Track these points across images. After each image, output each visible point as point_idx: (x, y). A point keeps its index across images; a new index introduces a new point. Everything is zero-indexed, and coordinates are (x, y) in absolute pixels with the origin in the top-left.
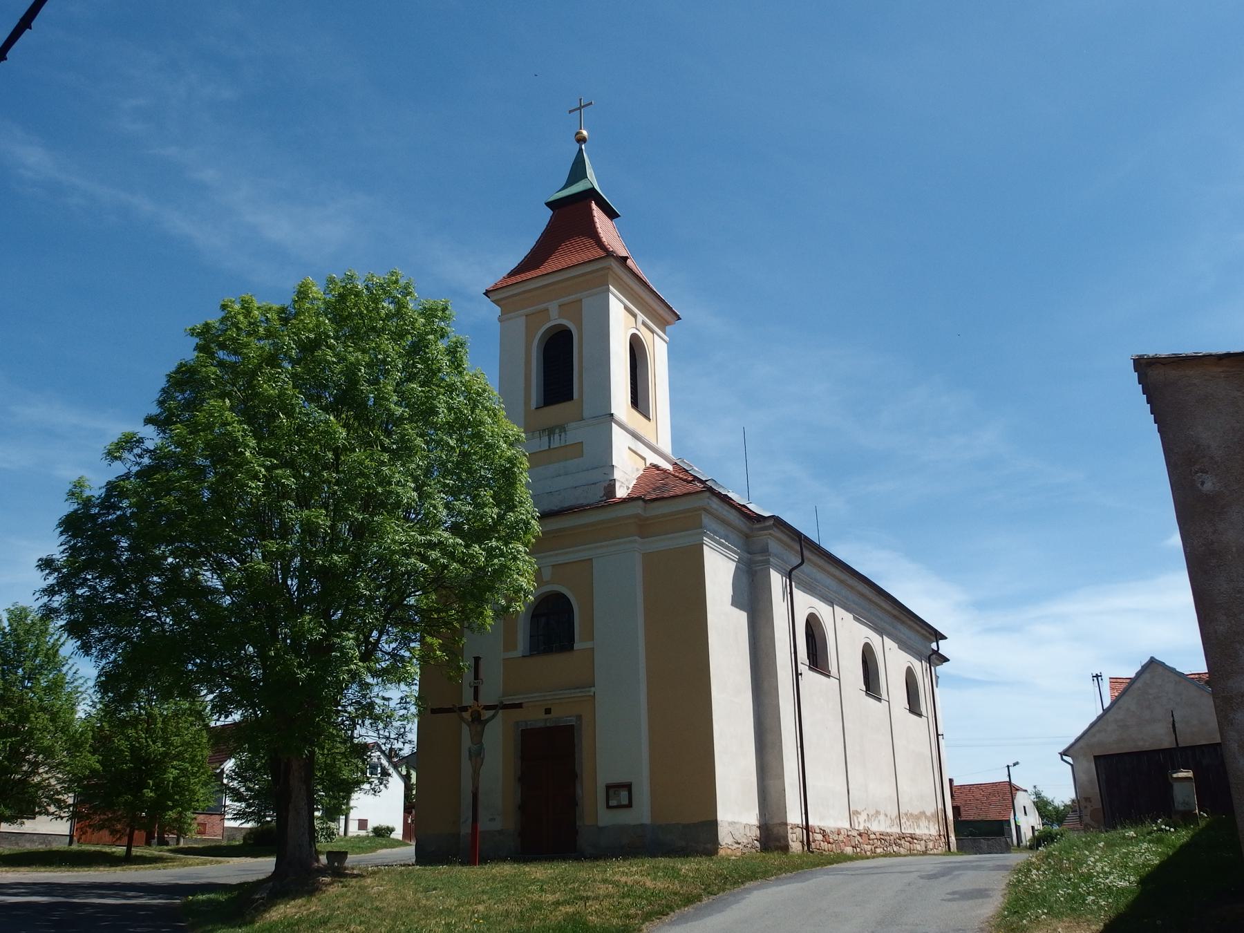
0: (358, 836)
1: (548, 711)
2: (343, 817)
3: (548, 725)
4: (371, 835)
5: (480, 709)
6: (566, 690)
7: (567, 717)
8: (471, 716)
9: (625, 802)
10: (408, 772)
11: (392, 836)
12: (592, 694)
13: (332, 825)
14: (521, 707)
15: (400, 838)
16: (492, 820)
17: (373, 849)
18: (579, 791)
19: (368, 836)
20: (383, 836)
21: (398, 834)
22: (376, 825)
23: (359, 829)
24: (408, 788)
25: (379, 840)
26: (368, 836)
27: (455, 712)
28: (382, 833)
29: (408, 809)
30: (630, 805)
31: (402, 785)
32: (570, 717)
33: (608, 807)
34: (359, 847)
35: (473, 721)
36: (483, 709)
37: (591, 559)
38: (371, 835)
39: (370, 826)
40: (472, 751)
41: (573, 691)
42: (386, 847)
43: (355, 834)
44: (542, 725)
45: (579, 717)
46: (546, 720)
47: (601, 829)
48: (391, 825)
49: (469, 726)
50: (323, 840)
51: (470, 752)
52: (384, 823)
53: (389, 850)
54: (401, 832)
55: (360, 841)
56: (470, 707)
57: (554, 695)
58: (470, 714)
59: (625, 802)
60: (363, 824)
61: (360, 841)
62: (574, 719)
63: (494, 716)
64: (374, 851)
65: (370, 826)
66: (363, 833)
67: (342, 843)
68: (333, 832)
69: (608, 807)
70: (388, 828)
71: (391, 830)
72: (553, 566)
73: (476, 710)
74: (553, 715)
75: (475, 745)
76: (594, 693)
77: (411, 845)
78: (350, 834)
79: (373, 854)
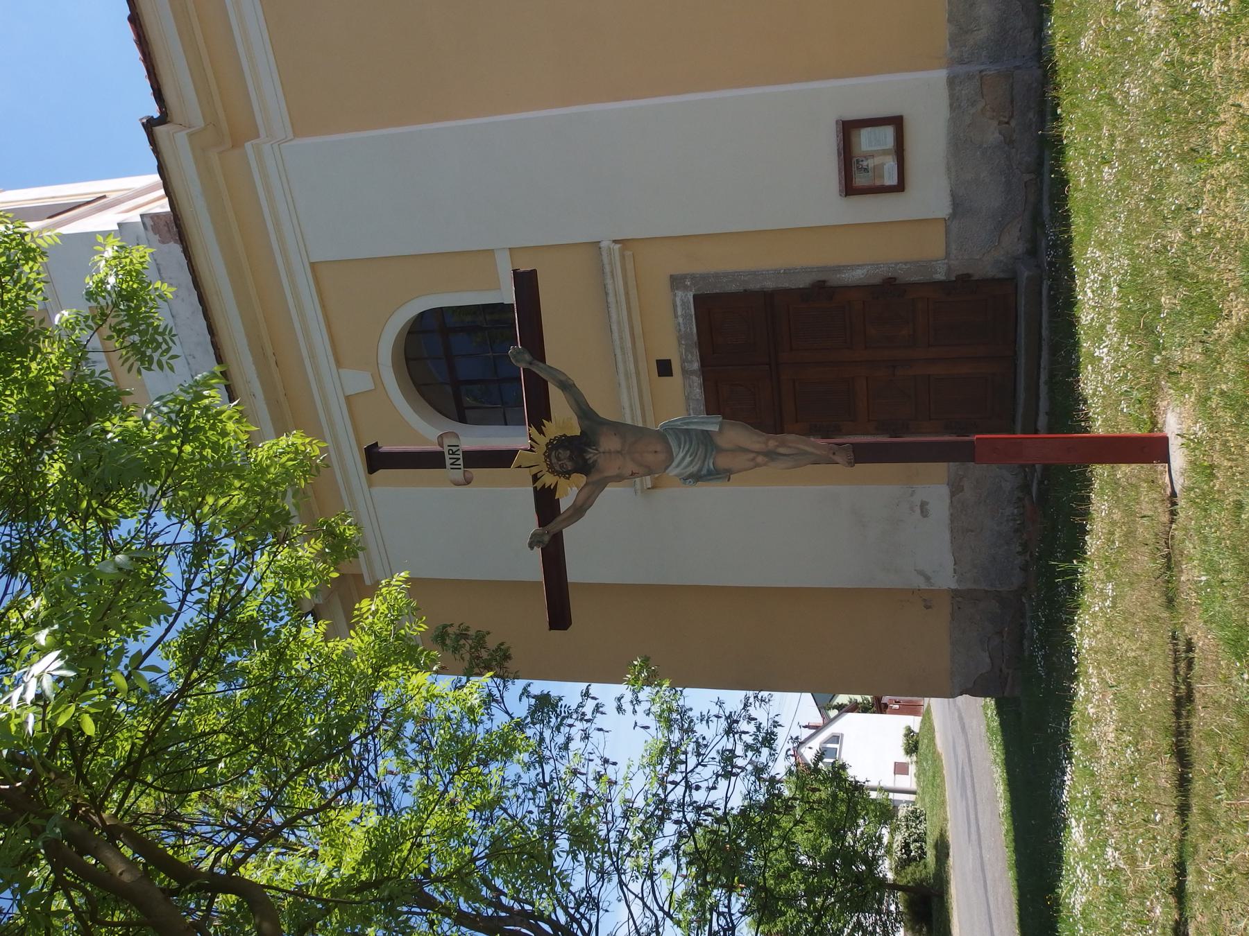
0: (918, 776)
1: (664, 368)
2: (891, 796)
3: (696, 366)
4: (914, 758)
5: (543, 441)
6: (610, 317)
7: (676, 317)
8: (566, 474)
9: (888, 133)
10: (835, 708)
11: (916, 729)
12: (617, 246)
13: (902, 812)
14: (533, 274)
15: (918, 719)
16: (924, 511)
17: (936, 758)
18: (857, 276)
19: (917, 762)
20: (917, 742)
21: (914, 722)
22: (902, 752)
23: (671, 375)
24: (854, 708)
25: (922, 747)
26: (917, 762)
27: (542, 523)
28: (912, 745)
29: (880, 707)
30: (897, 122)
31: (850, 715)
32: (675, 306)
33: (900, 187)
34: (934, 777)
35: (585, 468)
36: (541, 432)
37: (313, 265)
38: (914, 758)
39: (904, 758)
40: (693, 469)
41: (611, 299)
42: (932, 739)
43: (914, 779)
44: (697, 381)
45: (676, 282)
46: (685, 372)
47: (959, 206)
48: (903, 732)
49: (601, 485)
50: (922, 827)
51: (697, 477)
52: (899, 742)
53: (937, 735)
54: (911, 717)
55: (925, 774)
56: (535, 478)
57: (622, 348)
58: (562, 482)
59: (888, 133)
60: (900, 769)
61: (925, 774)
62: (680, 293)
63: (567, 387)
64: (939, 756)
65: (904, 758)
66: (913, 769)
67: (927, 800)
68: (912, 812)
69: (900, 187)
70: (906, 735)
71: (909, 732)
72: (339, 363)
73: (547, 456)
74: (671, 352)
75: (671, 458)
76: (615, 242)
77: (929, 705)
78: (914, 787)
79: (943, 757)
